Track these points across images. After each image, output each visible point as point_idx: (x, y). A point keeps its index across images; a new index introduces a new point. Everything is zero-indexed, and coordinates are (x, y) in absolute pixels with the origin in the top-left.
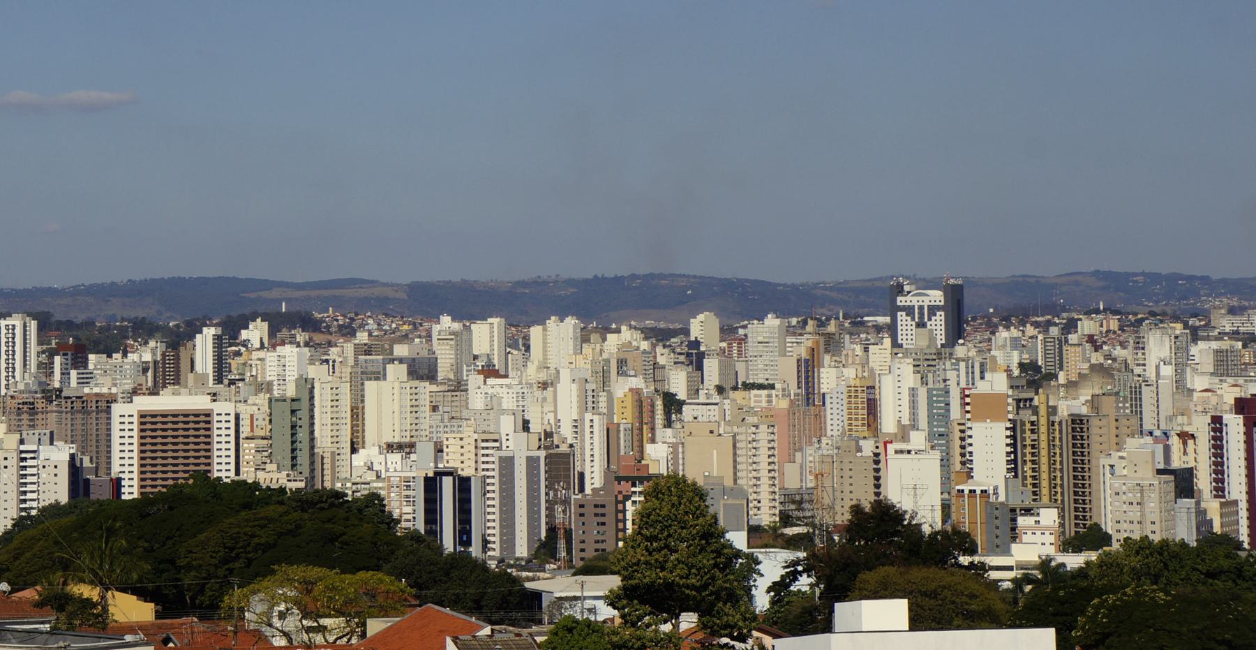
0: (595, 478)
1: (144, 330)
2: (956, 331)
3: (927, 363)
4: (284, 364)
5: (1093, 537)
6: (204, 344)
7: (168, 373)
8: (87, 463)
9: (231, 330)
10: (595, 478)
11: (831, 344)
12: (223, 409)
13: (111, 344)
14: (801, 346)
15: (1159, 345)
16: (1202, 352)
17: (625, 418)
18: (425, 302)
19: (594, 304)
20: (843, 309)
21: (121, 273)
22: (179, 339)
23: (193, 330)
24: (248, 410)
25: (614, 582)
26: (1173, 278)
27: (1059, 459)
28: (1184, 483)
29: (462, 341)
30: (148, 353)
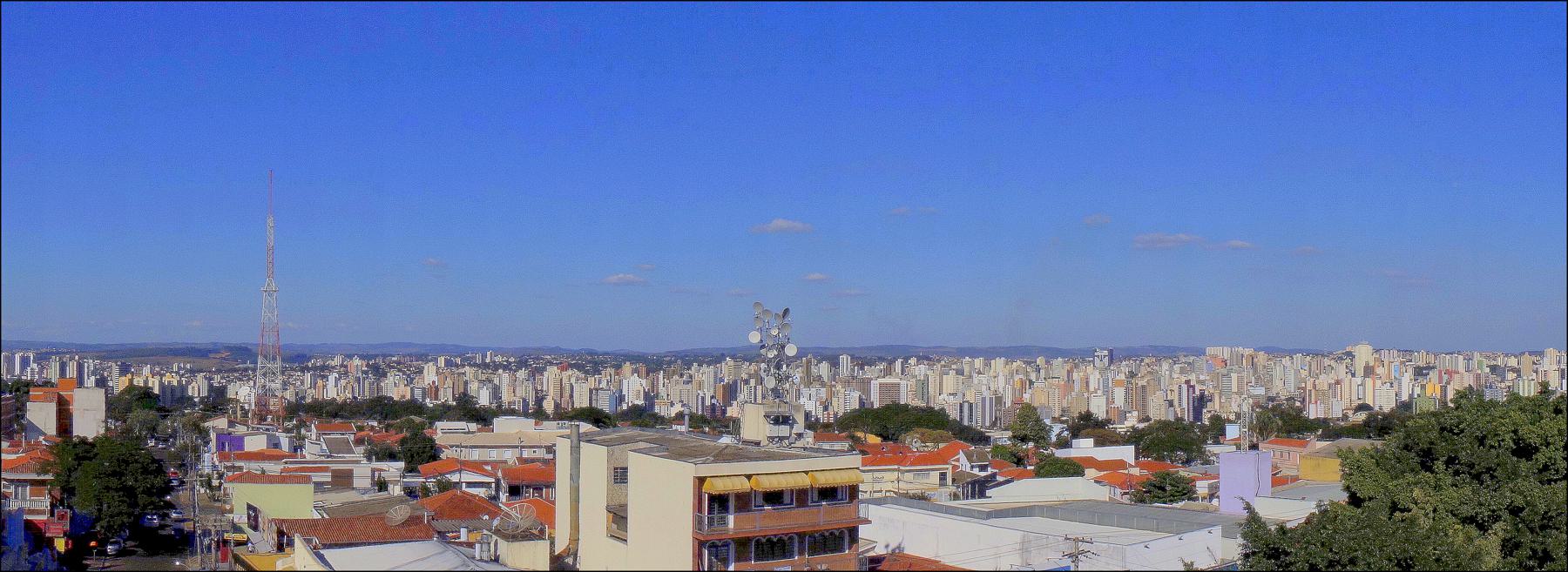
0: (1009, 404)
1: (881, 359)
2: (1111, 361)
3: (1103, 371)
4: (921, 370)
5: (1147, 419)
6: (898, 363)
7: (888, 372)
8: (726, 440)
9: (906, 359)
10: (1009, 404)
11: (1076, 366)
12: (903, 383)
13: (871, 363)
14: (1067, 367)
15: (1165, 366)
16: (1177, 367)
17: (1018, 386)
18: (962, 352)
19: (1010, 354)
20: (1079, 356)
21: (875, 344)
22: (891, 363)
23: (895, 360)
24: (907, 385)
25: (1010, 433)
26: (1169, 348)
27: (1138, 397)
28: (1171, 404)
29: (972, 364)
30: (882, 366)
